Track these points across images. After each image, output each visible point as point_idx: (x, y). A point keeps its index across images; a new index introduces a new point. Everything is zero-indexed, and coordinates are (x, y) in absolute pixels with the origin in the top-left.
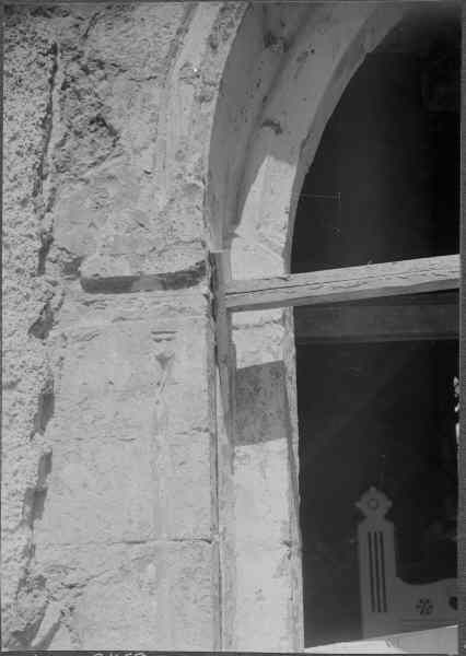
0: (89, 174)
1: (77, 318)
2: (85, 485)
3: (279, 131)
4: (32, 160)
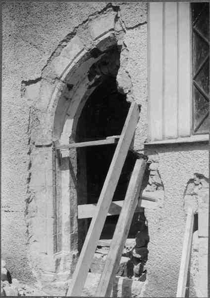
0: (36, 128)
1: (35, 151)
2: (141, 16)
3: (69, 116)
4: (27, 126)
